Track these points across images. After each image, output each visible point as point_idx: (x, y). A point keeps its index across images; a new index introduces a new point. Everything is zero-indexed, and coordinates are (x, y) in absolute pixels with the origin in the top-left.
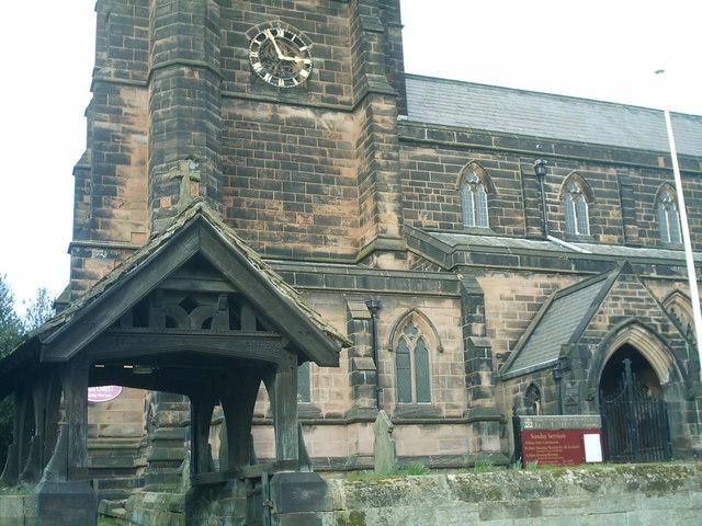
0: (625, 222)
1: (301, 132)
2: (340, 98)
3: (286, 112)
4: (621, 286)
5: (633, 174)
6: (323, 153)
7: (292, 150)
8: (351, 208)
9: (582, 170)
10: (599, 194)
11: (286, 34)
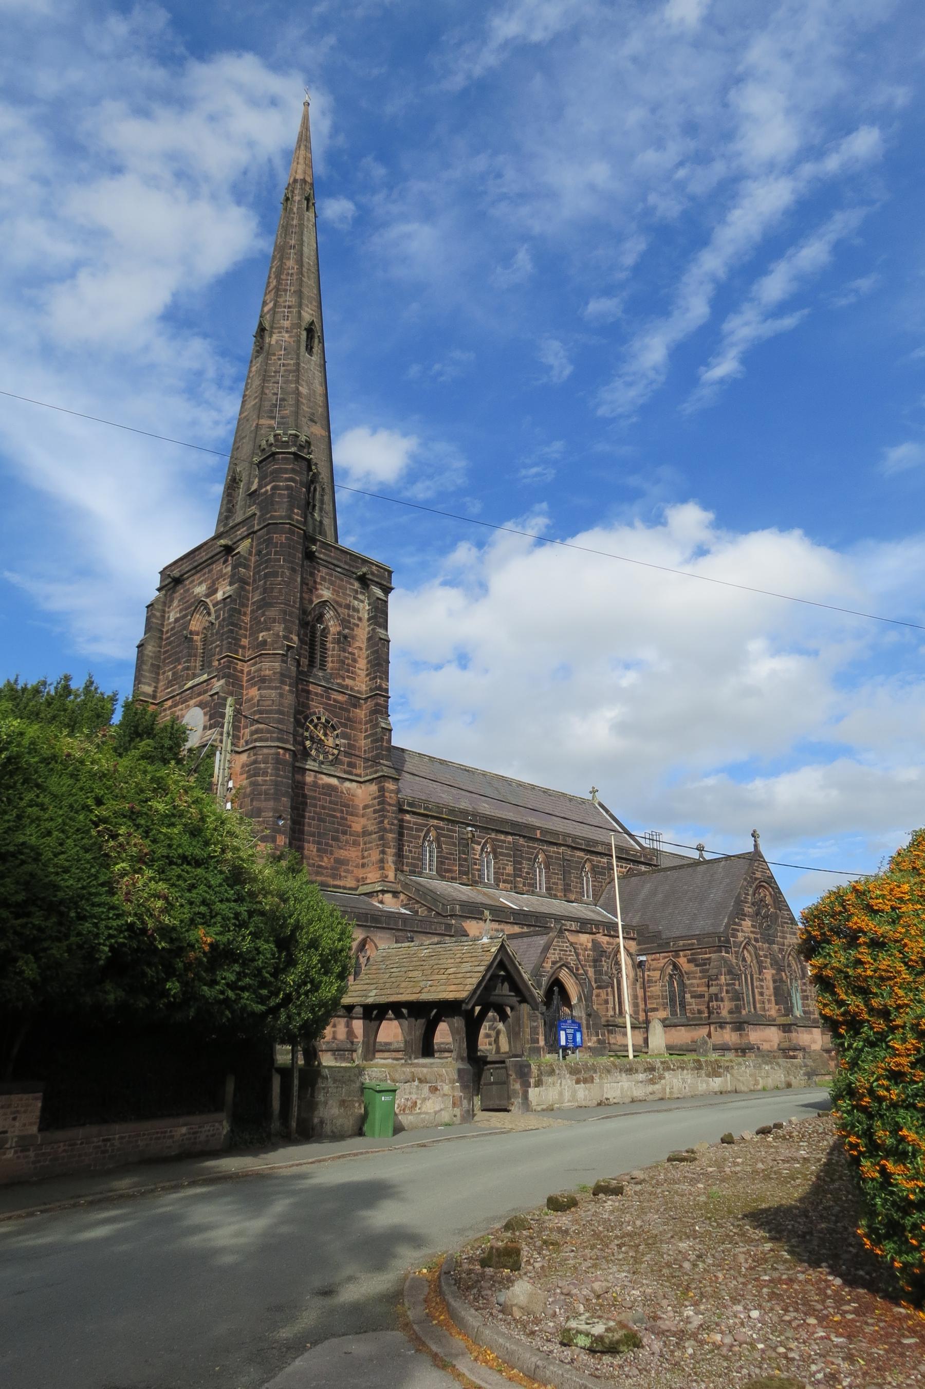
0: (515, 876)
1: (330, 795)
2: (354, 771)
3: (322, 779)
4: (558, 942)
5: (521, 841)
6: (342, 812)
7: (324, 808)
8: (356, 854)
9: (493, 836)
10: (502, 854)
11: (326, 720)
